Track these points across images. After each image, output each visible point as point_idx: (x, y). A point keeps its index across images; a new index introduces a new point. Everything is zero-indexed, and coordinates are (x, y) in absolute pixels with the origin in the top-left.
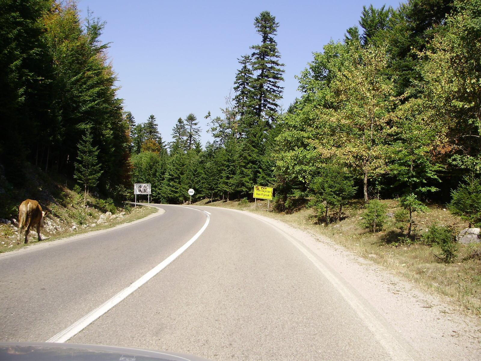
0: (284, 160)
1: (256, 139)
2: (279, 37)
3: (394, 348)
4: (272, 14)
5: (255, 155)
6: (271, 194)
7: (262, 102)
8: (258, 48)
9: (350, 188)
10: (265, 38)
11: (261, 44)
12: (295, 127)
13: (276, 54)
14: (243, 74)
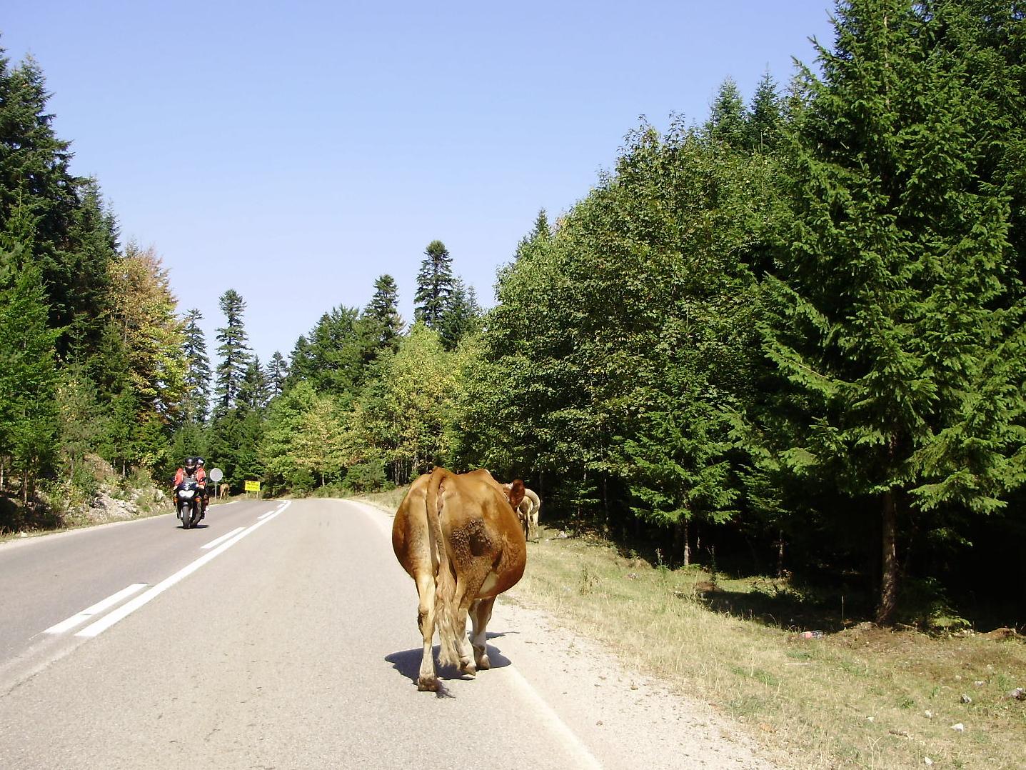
0: (273, 464)
1: (226, 432)
2: (245, 317)
3: (209, 437)
4: (239, 294)
5: (226, 449)
6: (259, 487)
7: (230, 389)
8: (222, 330)
9: (312, 480)
10: (232, 319)
11: (227, 326)
12: (278, 441)
13: (244, 336)
14: (190, 334)
